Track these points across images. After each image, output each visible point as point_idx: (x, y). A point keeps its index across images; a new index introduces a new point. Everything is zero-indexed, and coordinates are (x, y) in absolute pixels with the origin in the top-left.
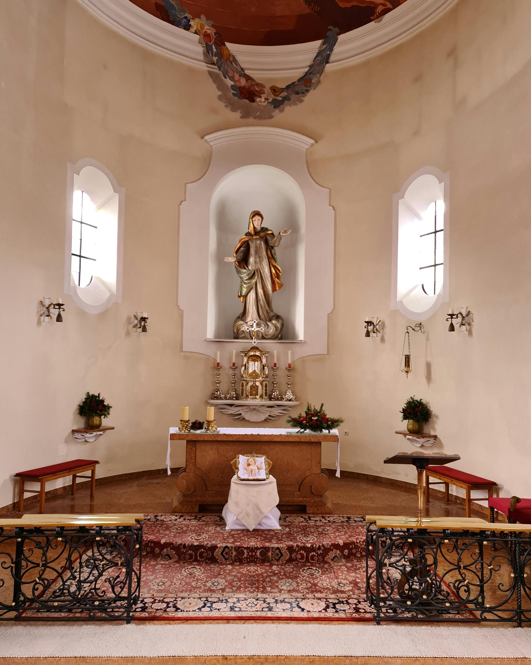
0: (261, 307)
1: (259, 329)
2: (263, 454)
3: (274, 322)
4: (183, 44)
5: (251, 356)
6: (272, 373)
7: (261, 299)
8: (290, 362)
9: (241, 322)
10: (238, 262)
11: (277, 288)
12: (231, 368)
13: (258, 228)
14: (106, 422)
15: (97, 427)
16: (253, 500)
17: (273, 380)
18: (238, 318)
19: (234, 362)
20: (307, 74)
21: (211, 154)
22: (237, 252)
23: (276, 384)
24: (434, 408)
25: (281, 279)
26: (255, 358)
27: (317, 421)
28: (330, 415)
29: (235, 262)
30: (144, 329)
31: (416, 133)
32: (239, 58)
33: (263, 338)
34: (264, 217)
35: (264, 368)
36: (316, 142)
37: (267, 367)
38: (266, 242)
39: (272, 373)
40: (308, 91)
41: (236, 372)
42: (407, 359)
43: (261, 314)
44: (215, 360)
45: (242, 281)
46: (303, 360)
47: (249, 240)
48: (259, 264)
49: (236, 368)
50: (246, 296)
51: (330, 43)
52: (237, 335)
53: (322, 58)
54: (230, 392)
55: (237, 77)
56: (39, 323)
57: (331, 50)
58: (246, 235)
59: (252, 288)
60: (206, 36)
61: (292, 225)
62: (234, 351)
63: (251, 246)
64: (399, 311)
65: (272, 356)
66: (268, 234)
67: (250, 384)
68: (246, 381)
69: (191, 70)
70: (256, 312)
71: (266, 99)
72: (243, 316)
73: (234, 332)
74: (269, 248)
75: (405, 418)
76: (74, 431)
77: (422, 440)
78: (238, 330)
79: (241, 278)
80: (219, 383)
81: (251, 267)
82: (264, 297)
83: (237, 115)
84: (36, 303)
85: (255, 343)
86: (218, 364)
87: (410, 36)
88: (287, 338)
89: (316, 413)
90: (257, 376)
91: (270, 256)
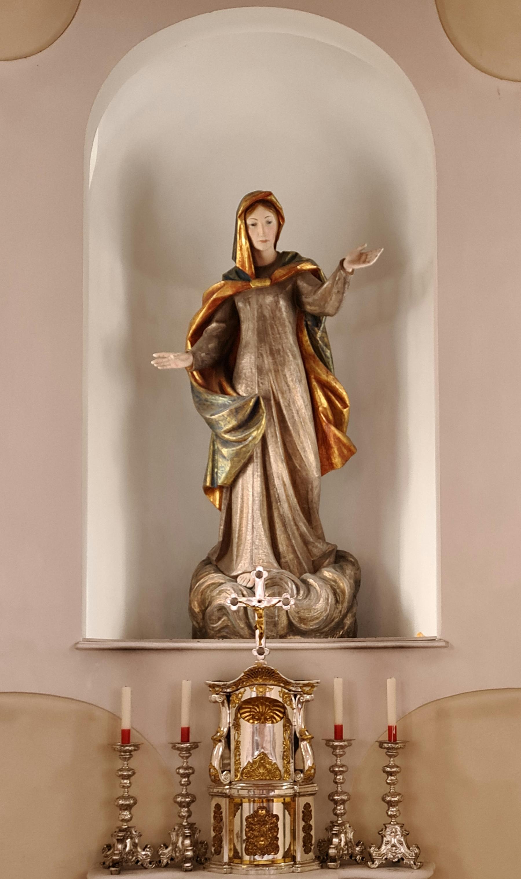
0: (284, 525)
1: (275, 600)
3: (327, 573)
5: (250, 701)
6: (327, 761)
7: (283, 497)
8: (392, 721)
9: (215, 577)
10: (201, 373)
11: (337, 460)
12: (174, 747)
13: (268, 255)
17: (332, 788)
18: (207, 562)
19: (184, 724)
23: (343, 802)
25: (349, 429)
26: (264, 710)
29: (189, 370)
33: (293, 630)
34: (280, 198)
35: (296, 746)
37: (310, 740)
38: (296, 301)
39: (327, 761)
41: (193, 762)
43: (283, 547)
44: (116, 718)
45: (217, 437)
46: (441, 711)
47: (237, 293)
48: (272, 377)
49: (196, 746)
50: (229, 488)
52: (203, 625)
58: (226, 277)
59: (250, 460)
62: (186, 686)
63: (242, 315)
65: (327, 697)
66: (302, 273)
67: (247, 809)
68: (230, 797)
70: (268, 550)
72: (222, 555)
73: (191, 610)
74: (308, 322)
78: (205, 605)
79: (211, 424)
80: (128, 808)
81: (246, 388)
82: (291, 491)
85: (261, 652)
86: (126, 735)
88: (371, 633)
90: (273, 775)
91: (311, 349)
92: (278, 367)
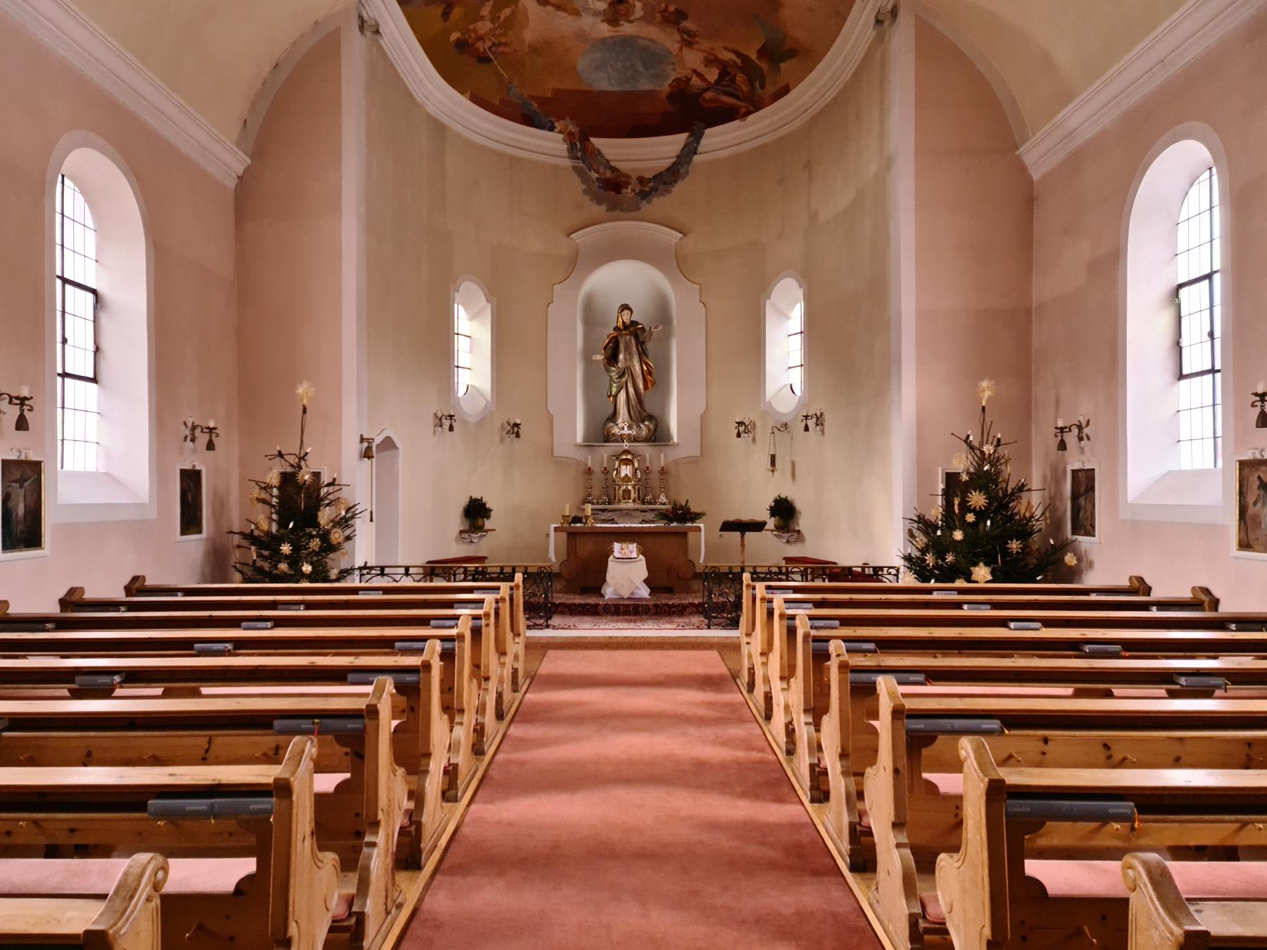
2: (634, 541)
4: (549, 145)
13: (628, 322)
14: (488, 524)
15: (480, 528)
16: (627, 573)
20: (674, 164)
21: (577, 253)
22: (605, 349)
24: (799, 505)
26: (627, 462)
27: (683, 514)
28: (694, 508)
30: (518, 435)
31: (780, 235)
32: (604, 151)
33: (635, 440)
34: (632, 306)
36: (685, 235)
38: (637, 337)
40: (676, 181)
42: (773, 457)
44: (586, 464)
46: (677, 463)
50: (616, 396)
51: (697, 137)
52: (608, 438)
53: (690, 151)
54: (602, 490)
55: (602, 169)
56: (434, 433)
57: (698, 143)
60: (571, 134)
61: (664, 316)
64: (768, 412)
69: (555, 167)
71: (633, 190)
72: (613, 417)
74: (640, 343)
75: (773, 515)
76: (461, 532)
77: (786, 535)
78: (608, 433)
83: (603, 208)
84: (431, 418)
87: (774, 138)
88: (661, 440)
89: (681, 508)
92: (631, 358)
